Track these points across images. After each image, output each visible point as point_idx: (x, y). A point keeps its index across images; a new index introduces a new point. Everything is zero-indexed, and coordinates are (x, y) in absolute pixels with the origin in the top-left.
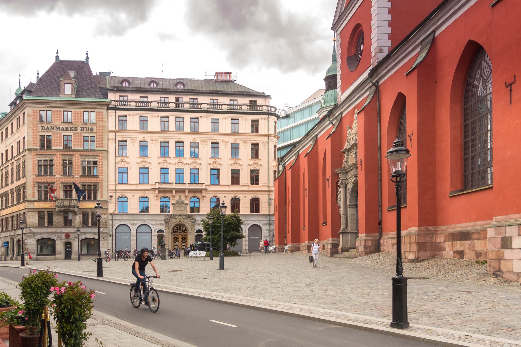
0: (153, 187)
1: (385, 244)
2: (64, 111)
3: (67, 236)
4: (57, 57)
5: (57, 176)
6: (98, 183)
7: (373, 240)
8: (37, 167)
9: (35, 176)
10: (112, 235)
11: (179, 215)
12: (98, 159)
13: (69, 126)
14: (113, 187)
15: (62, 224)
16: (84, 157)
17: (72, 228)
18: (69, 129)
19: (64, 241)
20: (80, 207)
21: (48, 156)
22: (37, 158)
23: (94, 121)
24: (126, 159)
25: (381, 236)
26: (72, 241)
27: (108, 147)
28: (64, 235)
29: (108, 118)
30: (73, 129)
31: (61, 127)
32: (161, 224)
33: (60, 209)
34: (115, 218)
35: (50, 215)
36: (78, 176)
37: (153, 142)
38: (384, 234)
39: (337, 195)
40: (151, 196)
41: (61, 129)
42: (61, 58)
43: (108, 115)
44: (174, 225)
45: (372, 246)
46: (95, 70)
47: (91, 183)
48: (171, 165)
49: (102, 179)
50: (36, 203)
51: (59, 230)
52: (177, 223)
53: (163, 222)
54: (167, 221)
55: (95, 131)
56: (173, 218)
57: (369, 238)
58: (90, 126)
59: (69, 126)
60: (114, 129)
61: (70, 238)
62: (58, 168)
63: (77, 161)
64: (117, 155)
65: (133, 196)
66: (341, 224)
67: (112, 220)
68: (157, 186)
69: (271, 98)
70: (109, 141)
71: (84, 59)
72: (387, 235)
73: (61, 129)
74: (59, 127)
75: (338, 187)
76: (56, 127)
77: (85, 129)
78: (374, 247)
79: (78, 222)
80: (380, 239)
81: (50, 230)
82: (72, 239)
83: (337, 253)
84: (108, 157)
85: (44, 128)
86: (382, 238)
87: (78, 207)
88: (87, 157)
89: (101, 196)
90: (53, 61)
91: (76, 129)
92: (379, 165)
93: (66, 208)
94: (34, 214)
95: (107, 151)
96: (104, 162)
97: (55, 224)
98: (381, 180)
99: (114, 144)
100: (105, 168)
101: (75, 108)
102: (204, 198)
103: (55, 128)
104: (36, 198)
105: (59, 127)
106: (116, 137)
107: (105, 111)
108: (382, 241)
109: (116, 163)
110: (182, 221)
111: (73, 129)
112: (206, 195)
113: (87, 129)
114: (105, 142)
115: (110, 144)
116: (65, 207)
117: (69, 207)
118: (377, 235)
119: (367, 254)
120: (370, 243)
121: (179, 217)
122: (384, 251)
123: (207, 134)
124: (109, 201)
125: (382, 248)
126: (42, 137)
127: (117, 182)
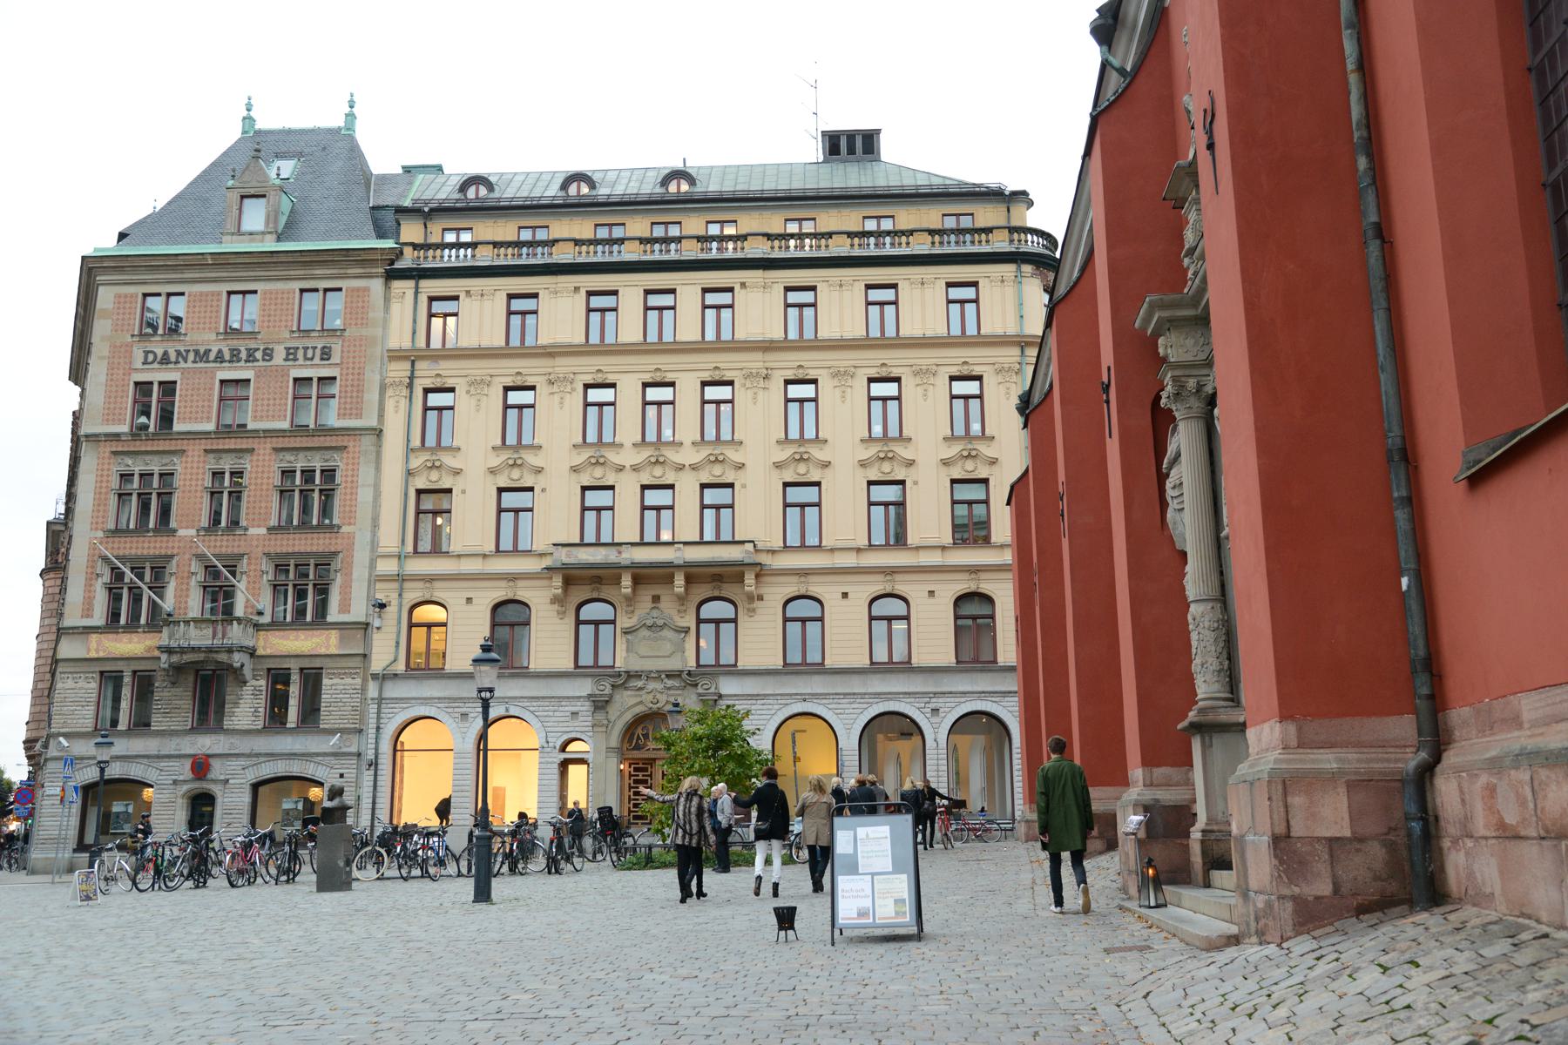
0: (547, 562)
1: (1481, 825)
2: (230, 293)
3: (201, 767)
4: (248, 120)
5: (181, 532)
6: (336, 554)
7: (1356, 785)
8: (113, 500)
9: (100, 534)
10: (374, 764)
11: (648, 676)
12: (339, 462)
13: (243, 346)
14: (387, 567)
15: (185, 719)
16: (289, 457)
17: (222, 737)
18: (243, 355)
19: (185, 788)
20: (260, 652)
21: (156, 458)
22: (116, 467)
23: (338, 323)
24: (448, 460)
25: (1437, 741)
26: (216, 790)
27: (381, 416)
28: (188, 764)
29: (387, 308)
30: (259, 355)
31: (215, 350)
32: (574, 714)
33: (175, 658)
34: (394, 690)
35: (144, 686)
36: (263, 531)
37: (555, 388)
38: (1458, 715)
39: (1162, 478)
40: (539, 598)
41: (212, 356)
42: (259, 125)
43: (387, 300)
44: (628, 717)
45: (1358, 839)
46: (383, 159)
47: (288, 554)
48: (622, 475)
49: (351, 536)
50: (94, 637)
51: (170, 746)
52: (639, 709)
53: (585, 708)
54: (600, 704)
55: (336, 359)
56: (623, 686)
57: (1327, 760)
58: (324, 343)
59: (243, 346)
60: (407, 344)
61: (211, 776)
62: (190, 503)
63: (262, 472)
64: (416, 442)
65: (469, 600)
66: (1196, 665)
67: (380, 700)
68: (563, 556)
69: (1031, 204)
70: (389, 392)
71: (339, 122)
72: (1490, 725)
73: (212, 356)
74: (207, 352)
75: (1162, 422)
76: (197, 352)
77: (300, 354)
78: (1377, 851)
79: (247, 708)
80: (1427, 771)
81: (138, 745)
82: (214, 781)
83: (1179, 875)
84: (379, 454)
85: (151, 357)
86: (1451, 758)
87: (252, 653)
88: (301, 455)
89: (345, 607)
90: (233, 134)
91: (268, 354)
92: (1356, 111)
93: (201, 657)
94: (82, 684)
95: (378, 433)
96: (366, 473)
97: (158, 722)
98: (1383, 233)
99: (404, 403)
100: (365, 495)
101: (269, 279)
102: (757, 604)
103: (191, 356)
104: (99, 618)
105: (207, 352)
106: (411, 378)
107: (377, 285)
108: (1447, 791)
109: (409, 473)
110: (663, 698)
111: (259, 355)
112: (764, 590)
113: (310, 354)
114: (372, 396)
115: (390, 405)
116: (193, 649)
117: (210, 650)
118: (1403, 727)
119: (1310, 917)
120: (1331, 816)
121: (652, 685)
122: (1482, 899)
123: (768, 347)
124: (377, 623)
125: (1457, 863)
126: (143, 388)
127: (410, 548)
